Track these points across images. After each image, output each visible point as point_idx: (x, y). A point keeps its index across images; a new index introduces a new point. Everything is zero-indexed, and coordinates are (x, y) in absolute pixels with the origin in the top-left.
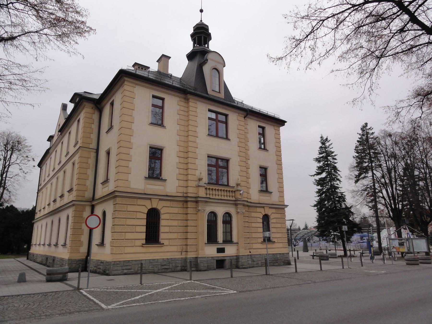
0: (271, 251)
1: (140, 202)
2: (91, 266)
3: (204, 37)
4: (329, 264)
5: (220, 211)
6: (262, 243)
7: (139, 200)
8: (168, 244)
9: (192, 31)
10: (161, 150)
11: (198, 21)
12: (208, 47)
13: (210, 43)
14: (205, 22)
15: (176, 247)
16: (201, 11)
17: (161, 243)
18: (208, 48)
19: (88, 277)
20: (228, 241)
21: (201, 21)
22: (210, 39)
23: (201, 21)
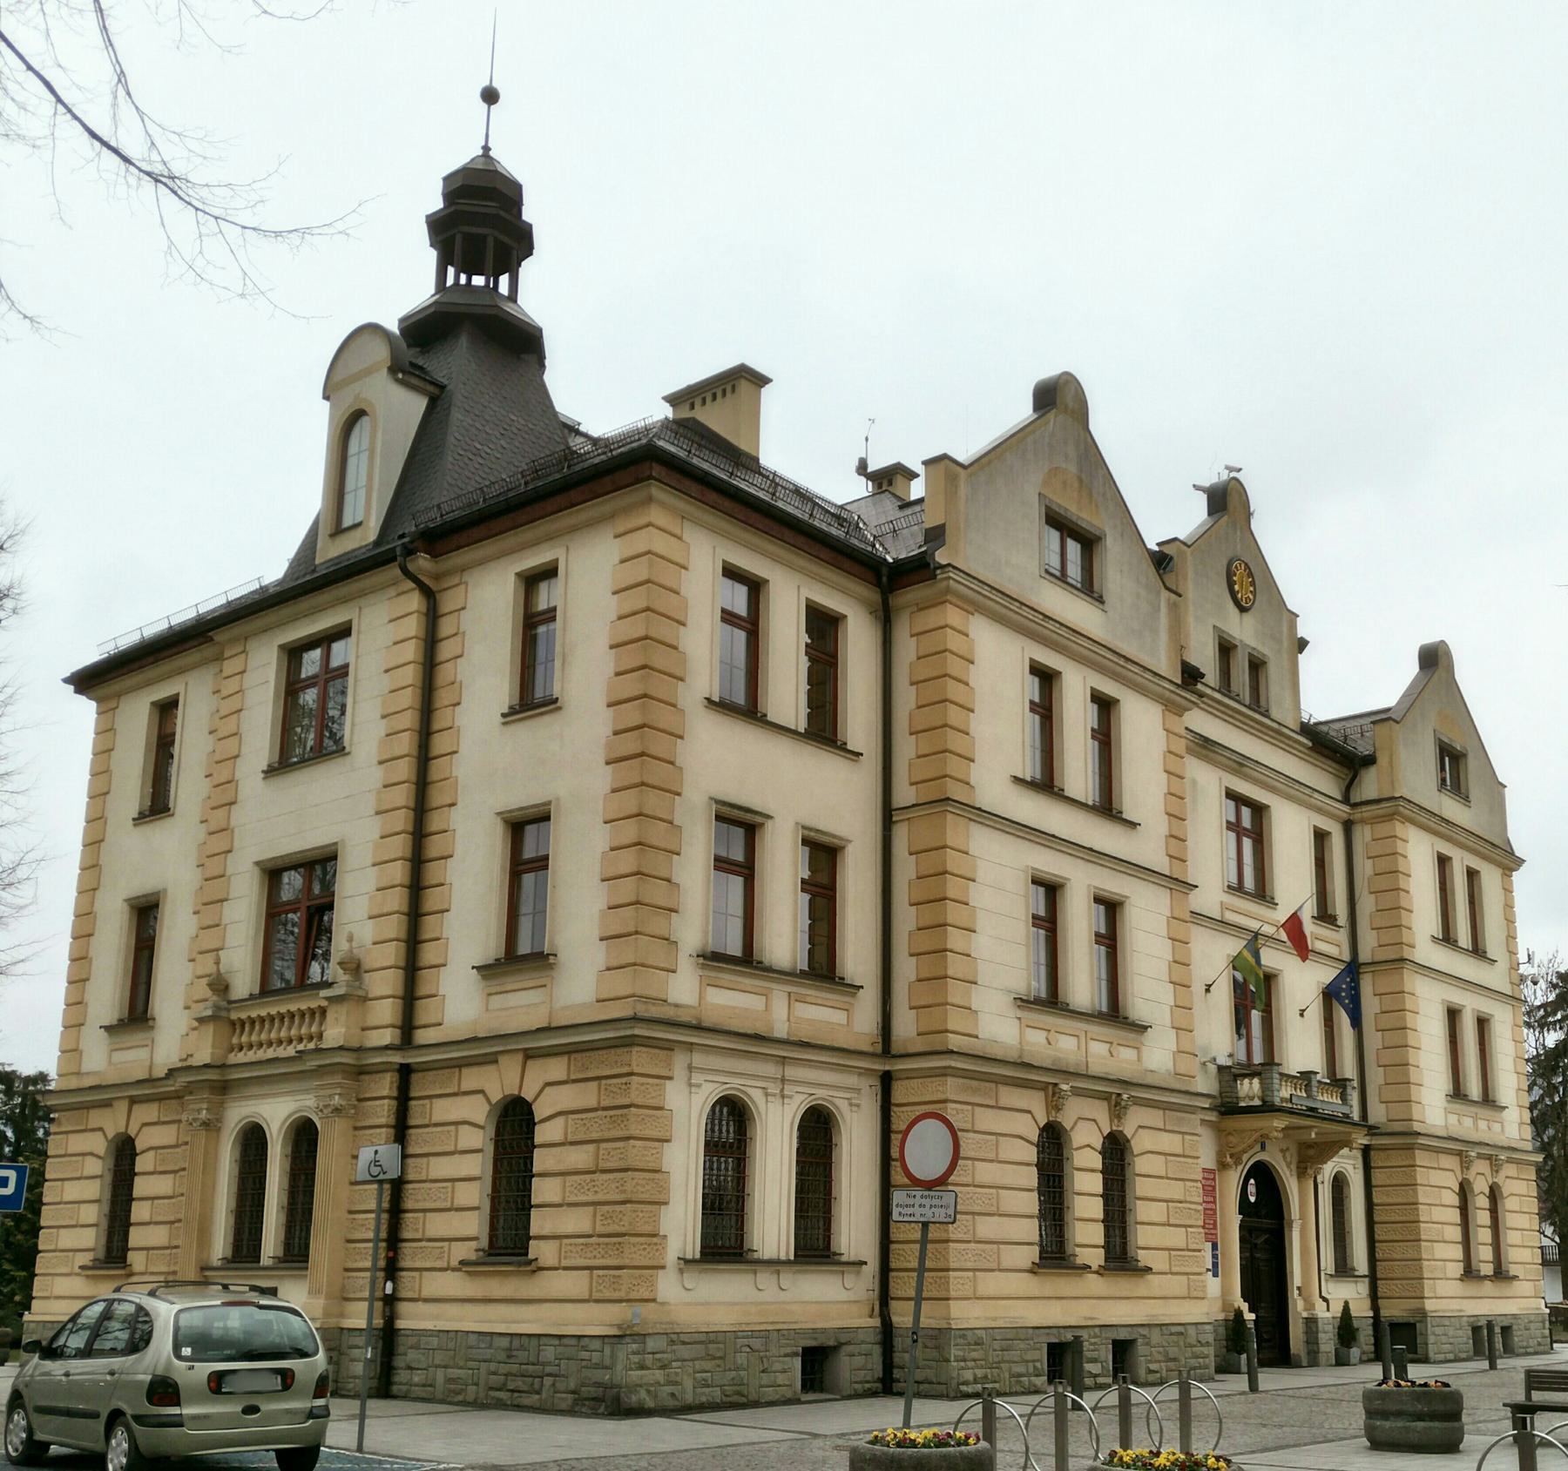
0: (529, 1321)
1: (1011, 1096)
2: (412, 1366)
3: (496, 240)
4: (598, 1384)
5: (274, 1113)
6: (1034, 1270)
7: (1003, 1090)
8: (1166, 1268)
9: (437, 204)
10: (1062, 886)
11: (462, 154)
12: (513, 297)
13: (527, 269)
14: (511, 162)
15: (425, 1293)
16: (490, 96)
17: (1079, 1261)
18: (515, 301)
19: (362, 1417)
20: (1120, 1257)
21: (486, 148)
22: (528, 250)
23: (486, 148)
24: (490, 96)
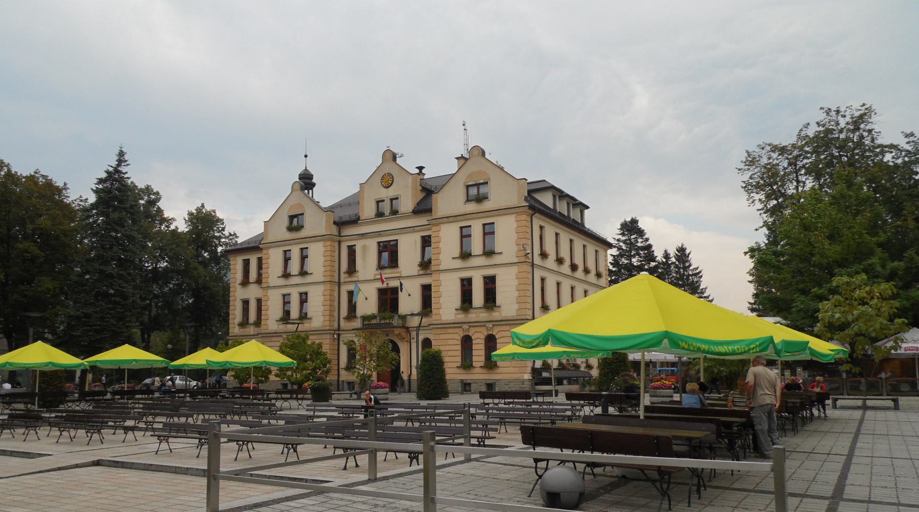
14: (312, 171)
24: (306, 156)
